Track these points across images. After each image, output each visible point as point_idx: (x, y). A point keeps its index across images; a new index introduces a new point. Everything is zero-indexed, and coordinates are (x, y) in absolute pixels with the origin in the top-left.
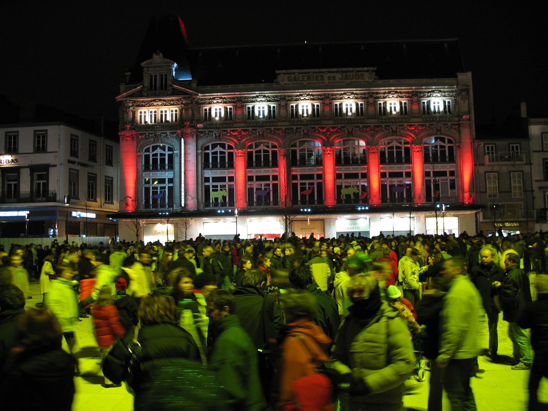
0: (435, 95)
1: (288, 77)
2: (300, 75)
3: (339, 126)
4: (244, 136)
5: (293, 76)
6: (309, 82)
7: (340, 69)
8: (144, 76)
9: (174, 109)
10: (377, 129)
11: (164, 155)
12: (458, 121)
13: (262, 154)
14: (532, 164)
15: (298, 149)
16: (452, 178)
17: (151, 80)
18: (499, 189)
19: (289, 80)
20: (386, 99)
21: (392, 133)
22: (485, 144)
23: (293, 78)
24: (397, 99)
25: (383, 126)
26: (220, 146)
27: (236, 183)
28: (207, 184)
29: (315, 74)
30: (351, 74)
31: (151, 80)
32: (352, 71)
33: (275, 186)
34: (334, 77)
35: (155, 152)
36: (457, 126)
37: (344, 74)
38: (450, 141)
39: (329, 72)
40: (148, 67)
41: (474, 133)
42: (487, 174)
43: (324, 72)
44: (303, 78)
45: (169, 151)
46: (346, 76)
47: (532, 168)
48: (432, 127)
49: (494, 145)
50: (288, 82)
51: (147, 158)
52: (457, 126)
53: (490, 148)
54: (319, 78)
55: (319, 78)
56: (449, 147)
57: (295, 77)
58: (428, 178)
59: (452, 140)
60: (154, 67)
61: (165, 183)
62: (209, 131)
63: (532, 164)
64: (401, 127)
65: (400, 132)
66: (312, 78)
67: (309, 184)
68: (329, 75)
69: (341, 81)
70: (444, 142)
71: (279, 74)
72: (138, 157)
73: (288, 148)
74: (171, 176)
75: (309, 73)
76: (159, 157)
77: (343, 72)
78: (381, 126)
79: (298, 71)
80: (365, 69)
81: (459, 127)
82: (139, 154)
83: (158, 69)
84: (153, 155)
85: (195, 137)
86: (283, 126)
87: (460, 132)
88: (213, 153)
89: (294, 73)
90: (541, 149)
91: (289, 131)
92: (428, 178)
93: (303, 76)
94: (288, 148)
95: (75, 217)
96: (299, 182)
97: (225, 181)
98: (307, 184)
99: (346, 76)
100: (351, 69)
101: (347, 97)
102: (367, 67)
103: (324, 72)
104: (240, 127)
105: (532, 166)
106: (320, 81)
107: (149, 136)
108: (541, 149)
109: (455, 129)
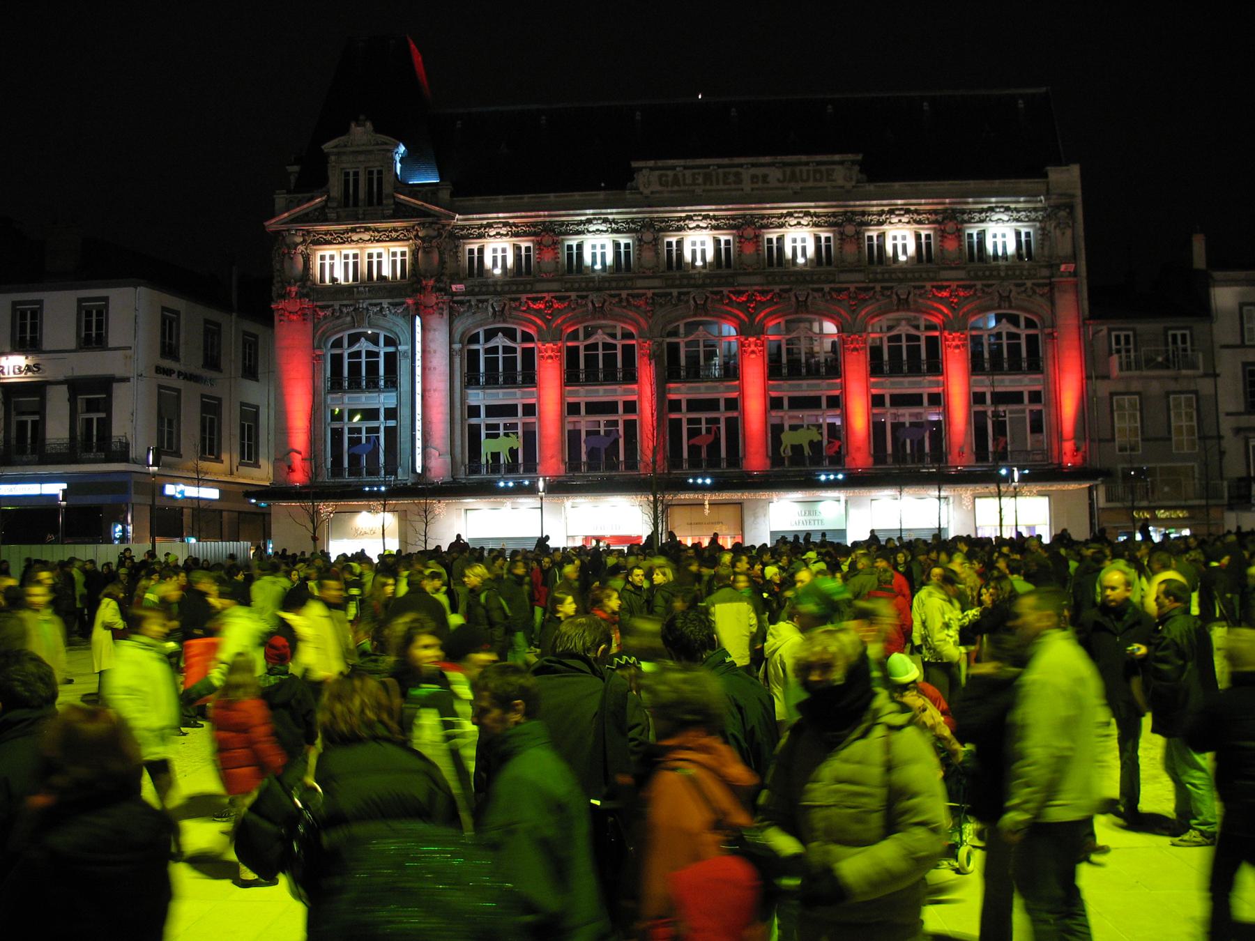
0: (995, 217)
1: (660, 177)
2: (688, 173)
3: (777, 289)
4: (560, 310)
5: (670, 173)
6: (708, 187)
7: (779, 159)
8: (330, 173)
9: (399, 250)
10: (863, 295)
11: (377, 355)
12: (1050, 278)
13: (600, 352)
14: (1218, 375)
15: (682, 341)
16: (1036, 407)
17: (347, 182)
18: (1142, 432)
19: (661, 184)
20: (885, 227)
21: (898, 305)
22: (1110, 330)
23: (670, 179)
24: (908, 226)
25: (878, 288)
26: (505, 335)
27: (539, 419)
28: (474, 421)
29: (720, 171)
30: (804, 168)
31: (347, 182)
32: (807, 164)
33: (630, 426)
34: (765, 177)
35: (355, 349)
36: (1046, 289)
37: (788, 170)
38: (1030, 324)
39: (753, 165)
40: (338, 154)
41: (1086, 304)
42: (1115, 398)
43: (741, 166)
44: (694, 179)
45: (386, 345)
46: (793, 173)
47: (1219, 385)
48: (990, 290)
49: (1131, 333)
50: (660, 188)
51: (337, 361)
52: (1046, 289)
53: (1122, 338)
54: (731, 178)
55: (731, 178)
56: (1028, 336)
57: (675, 175)
58: (979, 408)
59: (1036, 320)
60: (353, 152)
61: (378, 418)
62: (479, 301)
63: (1218, 375)
64: (918, 292)
65: (915, 301)
66: (714, 179)
67: (708, 421)
68: (753, 171)
69: (780, 185)
70: (1017, 324)
71: (640, 169)
72: (317, 359)
73: (660, 340)
74: (392, 403)
75: (708, 166)
76: (364, 360)
77: (785, 164)
78: (873, 288)
79: (682, 162)
80: (837, 158)
81: (1052, 290)
82: (318, 352)
83: (361, 158)
84: (351, 355)
85: (446, 313)
86: (649, 288)
87: (1053, 303)
88: (487, 351)
89: (673, 168)
90: (1239, 342)
91: (662, 301)
92: (979, 408)
93: (694, 175)
94: (660, 340)
95: (172, 497)
96: (684, 416)
97: (516, 415)
98: (703, 422)
99: (793, 173)
100: (804, 158)
101: (795, 222)
102: (840, 152)
103: (741, 166)
104: (549, 291)
105: (1219, 380)
106: (733, 186)
107: (341, 312)
108: (1239, 342)
109: (1042, 296)
